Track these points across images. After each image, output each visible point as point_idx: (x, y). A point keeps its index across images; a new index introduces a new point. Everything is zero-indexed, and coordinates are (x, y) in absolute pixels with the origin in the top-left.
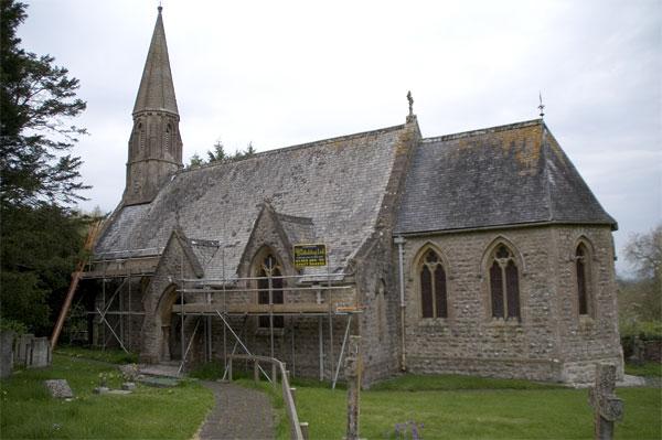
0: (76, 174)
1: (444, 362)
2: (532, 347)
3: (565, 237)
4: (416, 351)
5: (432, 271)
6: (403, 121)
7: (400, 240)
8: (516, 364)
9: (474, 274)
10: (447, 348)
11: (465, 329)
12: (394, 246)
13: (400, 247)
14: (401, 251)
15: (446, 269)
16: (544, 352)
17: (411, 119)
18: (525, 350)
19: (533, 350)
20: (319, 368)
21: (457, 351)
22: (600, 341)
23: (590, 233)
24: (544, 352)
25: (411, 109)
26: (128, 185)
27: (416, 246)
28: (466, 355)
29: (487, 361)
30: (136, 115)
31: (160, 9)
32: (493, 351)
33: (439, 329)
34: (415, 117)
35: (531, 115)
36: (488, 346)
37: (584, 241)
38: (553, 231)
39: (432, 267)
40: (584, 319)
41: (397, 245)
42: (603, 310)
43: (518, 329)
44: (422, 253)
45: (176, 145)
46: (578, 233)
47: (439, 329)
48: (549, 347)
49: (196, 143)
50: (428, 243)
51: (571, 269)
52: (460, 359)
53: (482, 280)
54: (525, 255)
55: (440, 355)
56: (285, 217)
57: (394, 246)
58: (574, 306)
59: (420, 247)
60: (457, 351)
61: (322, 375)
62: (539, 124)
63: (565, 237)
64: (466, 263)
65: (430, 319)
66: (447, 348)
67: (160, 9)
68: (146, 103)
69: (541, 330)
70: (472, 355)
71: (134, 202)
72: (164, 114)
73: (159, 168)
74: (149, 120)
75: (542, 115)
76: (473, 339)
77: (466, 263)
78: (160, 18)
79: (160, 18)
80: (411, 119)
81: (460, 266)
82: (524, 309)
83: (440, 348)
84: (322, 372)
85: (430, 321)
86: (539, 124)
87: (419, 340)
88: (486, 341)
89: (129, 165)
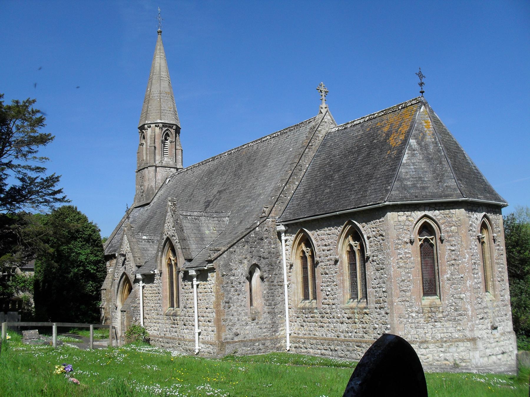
0: (59, 191)
1: (314, 342)
2: (245, 298)
11: (328, 311)
19: (375, 331)
20: (194, 341)
21: (323, 331)
22: (447, 324)
28: (329, 336)
29: (343, 341)
37: (428, 221)
40: (428, 300)
42: (452, 291)
43: (365, 310)
52: (325, 339)
55: (312, 336)
59: (342, 229)
61: (197, 347)
64: (328, 248)
65: (307, 301)
66: (317, 328)
70: (330, 335)
72: (161, 125)
76: (335, 320)
77: (328, 248)
83: (312, 329)
84: (197, 345)
85: (307, 303)
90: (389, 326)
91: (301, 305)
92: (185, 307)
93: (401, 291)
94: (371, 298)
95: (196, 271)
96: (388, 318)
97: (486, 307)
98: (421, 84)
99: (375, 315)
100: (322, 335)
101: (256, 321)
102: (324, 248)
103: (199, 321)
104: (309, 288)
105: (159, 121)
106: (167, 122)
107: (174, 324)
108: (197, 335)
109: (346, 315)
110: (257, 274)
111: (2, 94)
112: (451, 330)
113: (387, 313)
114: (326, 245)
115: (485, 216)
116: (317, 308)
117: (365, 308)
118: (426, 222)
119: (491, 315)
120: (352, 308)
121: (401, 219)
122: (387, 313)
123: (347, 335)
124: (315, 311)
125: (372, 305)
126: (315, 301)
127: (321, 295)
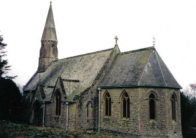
2: (132, 129)
3: (145, 91)
4: (103, 127)
5: (126, 100)
6: (113, 47)
7: (99, 89)
8: (128, 135)
9: (118, 101)
10: (110, 127)
12: (98, 91)
13: (100, 91)
14: (100, 92)
15: (112, 99)
16: (135, 131)
17: (116, 45)
18: (130, 130)
21: (113, 128)
23: (156, 91)
24: (135, 131)
25: (116, 42)
26: (39, 65)
27: (104, 91)
30: (42, 42)
31: (51, 2)
32: (122, 129)
33: (109, 120)
34: (117, 45)
35: (151, 45)
36: (121, 127)
38: (139, 89)
39: (108, 98)
41: (99, 90)
43: (129, 122)
44: (105, 94)
45: (55, 51)
46: (150, 90)
47: (109, 120)
48: (137, 130)
49: (63, 53)
50: (125, 90)
51: (147, 103)
53: (120, 104)
54: (131, 96)
56: (64, 80)
57: (98, 91)
58: (147, 116)
59: (122, 91)
60: (113, 128)
62: (153, 49)
63: (145, 91)
65: (107, 116)
66: (110, 127)
67: (51, 2)
68: (45, 37)
69: (135, 123)
70: (116, 130)
71: (40, 71)
73: (49, 60)
74: (46, 43)
75: (154, 45)
78: (51, 6)
79: (51, 6)
80: (116, 45)
81: (115, 99)
82: (131, 115)
86: (153, 49)
87: (104, 123)
88: (120, 125)
89: (40, 58)
90: (137, 129)
91: (105, 117)
92: (63, 116)
93: (142, 117)
94: (131, 118)
95: (68, 103)
96: (137, 126)
97: (172, 125)
98: (154, 42)
99: (132, 124)
100: (73, 125)
101: (89, 122)
102: (115, 98)
103: (68, 121)
104: (108, 112)
105: (49, 39)
106: (52, 40)
107: (57, 121)
108: (67, 126)
109: (122, 123)
110: (90, 105)
111: (1, 35)
112: (160, 132)
113: (137, 124)
114: (115, 97)
115: (174, 92)
116: (111, 119)
117: (129, 121)
118: (152, 93)
119: (174, 128)
120: (124, 121)
121: (143, 91)
122: (137, 124)
123: (122, 130)
124: (110, 120)
125: (132, 120)
126: (110, 116)
127: (112, 114)
